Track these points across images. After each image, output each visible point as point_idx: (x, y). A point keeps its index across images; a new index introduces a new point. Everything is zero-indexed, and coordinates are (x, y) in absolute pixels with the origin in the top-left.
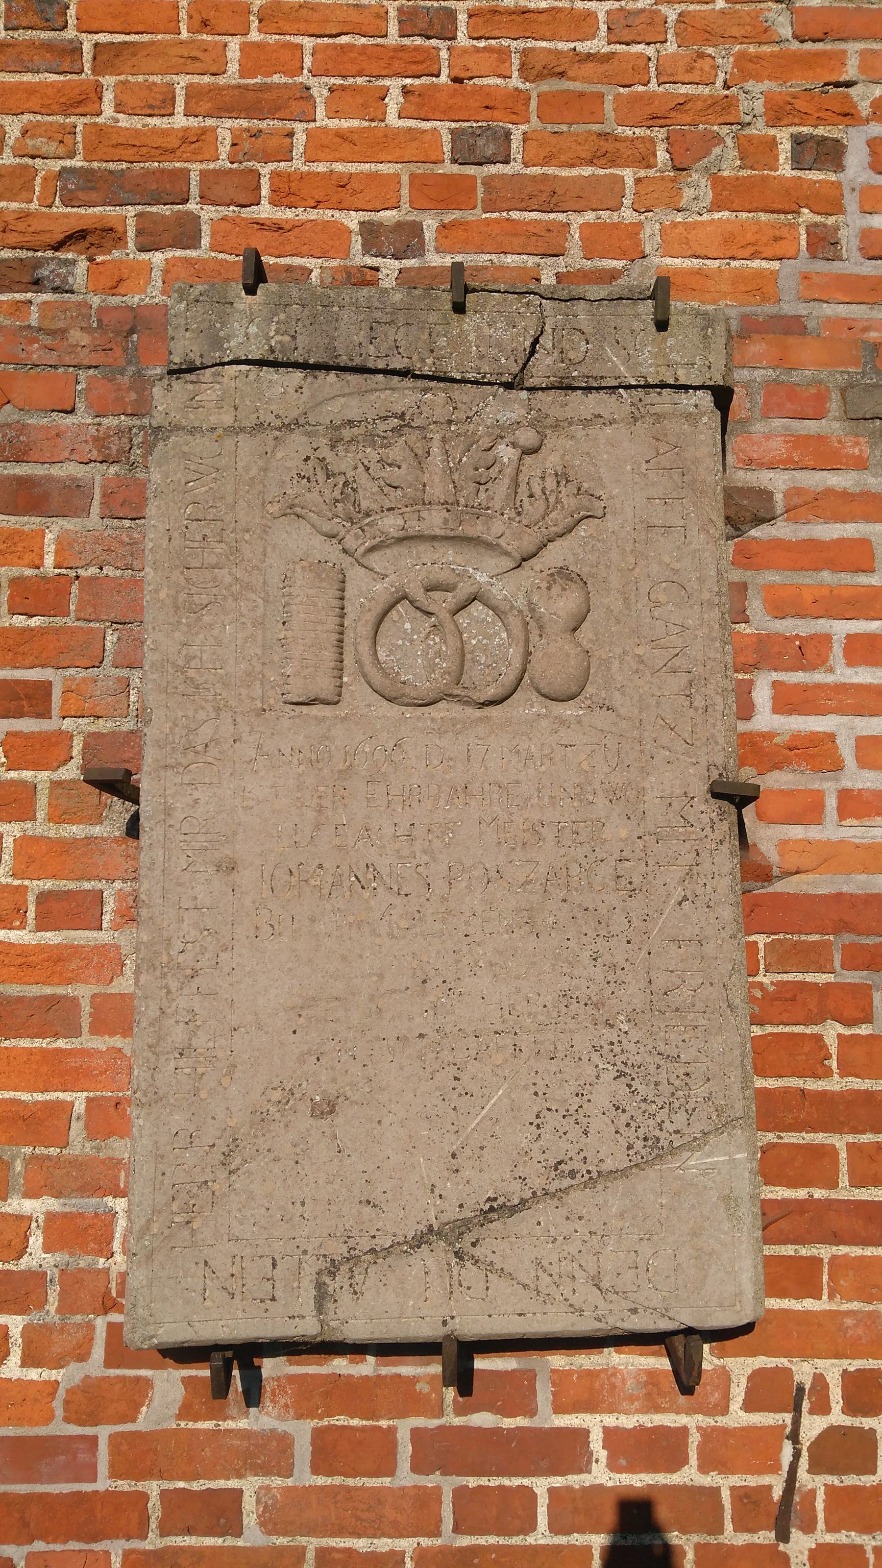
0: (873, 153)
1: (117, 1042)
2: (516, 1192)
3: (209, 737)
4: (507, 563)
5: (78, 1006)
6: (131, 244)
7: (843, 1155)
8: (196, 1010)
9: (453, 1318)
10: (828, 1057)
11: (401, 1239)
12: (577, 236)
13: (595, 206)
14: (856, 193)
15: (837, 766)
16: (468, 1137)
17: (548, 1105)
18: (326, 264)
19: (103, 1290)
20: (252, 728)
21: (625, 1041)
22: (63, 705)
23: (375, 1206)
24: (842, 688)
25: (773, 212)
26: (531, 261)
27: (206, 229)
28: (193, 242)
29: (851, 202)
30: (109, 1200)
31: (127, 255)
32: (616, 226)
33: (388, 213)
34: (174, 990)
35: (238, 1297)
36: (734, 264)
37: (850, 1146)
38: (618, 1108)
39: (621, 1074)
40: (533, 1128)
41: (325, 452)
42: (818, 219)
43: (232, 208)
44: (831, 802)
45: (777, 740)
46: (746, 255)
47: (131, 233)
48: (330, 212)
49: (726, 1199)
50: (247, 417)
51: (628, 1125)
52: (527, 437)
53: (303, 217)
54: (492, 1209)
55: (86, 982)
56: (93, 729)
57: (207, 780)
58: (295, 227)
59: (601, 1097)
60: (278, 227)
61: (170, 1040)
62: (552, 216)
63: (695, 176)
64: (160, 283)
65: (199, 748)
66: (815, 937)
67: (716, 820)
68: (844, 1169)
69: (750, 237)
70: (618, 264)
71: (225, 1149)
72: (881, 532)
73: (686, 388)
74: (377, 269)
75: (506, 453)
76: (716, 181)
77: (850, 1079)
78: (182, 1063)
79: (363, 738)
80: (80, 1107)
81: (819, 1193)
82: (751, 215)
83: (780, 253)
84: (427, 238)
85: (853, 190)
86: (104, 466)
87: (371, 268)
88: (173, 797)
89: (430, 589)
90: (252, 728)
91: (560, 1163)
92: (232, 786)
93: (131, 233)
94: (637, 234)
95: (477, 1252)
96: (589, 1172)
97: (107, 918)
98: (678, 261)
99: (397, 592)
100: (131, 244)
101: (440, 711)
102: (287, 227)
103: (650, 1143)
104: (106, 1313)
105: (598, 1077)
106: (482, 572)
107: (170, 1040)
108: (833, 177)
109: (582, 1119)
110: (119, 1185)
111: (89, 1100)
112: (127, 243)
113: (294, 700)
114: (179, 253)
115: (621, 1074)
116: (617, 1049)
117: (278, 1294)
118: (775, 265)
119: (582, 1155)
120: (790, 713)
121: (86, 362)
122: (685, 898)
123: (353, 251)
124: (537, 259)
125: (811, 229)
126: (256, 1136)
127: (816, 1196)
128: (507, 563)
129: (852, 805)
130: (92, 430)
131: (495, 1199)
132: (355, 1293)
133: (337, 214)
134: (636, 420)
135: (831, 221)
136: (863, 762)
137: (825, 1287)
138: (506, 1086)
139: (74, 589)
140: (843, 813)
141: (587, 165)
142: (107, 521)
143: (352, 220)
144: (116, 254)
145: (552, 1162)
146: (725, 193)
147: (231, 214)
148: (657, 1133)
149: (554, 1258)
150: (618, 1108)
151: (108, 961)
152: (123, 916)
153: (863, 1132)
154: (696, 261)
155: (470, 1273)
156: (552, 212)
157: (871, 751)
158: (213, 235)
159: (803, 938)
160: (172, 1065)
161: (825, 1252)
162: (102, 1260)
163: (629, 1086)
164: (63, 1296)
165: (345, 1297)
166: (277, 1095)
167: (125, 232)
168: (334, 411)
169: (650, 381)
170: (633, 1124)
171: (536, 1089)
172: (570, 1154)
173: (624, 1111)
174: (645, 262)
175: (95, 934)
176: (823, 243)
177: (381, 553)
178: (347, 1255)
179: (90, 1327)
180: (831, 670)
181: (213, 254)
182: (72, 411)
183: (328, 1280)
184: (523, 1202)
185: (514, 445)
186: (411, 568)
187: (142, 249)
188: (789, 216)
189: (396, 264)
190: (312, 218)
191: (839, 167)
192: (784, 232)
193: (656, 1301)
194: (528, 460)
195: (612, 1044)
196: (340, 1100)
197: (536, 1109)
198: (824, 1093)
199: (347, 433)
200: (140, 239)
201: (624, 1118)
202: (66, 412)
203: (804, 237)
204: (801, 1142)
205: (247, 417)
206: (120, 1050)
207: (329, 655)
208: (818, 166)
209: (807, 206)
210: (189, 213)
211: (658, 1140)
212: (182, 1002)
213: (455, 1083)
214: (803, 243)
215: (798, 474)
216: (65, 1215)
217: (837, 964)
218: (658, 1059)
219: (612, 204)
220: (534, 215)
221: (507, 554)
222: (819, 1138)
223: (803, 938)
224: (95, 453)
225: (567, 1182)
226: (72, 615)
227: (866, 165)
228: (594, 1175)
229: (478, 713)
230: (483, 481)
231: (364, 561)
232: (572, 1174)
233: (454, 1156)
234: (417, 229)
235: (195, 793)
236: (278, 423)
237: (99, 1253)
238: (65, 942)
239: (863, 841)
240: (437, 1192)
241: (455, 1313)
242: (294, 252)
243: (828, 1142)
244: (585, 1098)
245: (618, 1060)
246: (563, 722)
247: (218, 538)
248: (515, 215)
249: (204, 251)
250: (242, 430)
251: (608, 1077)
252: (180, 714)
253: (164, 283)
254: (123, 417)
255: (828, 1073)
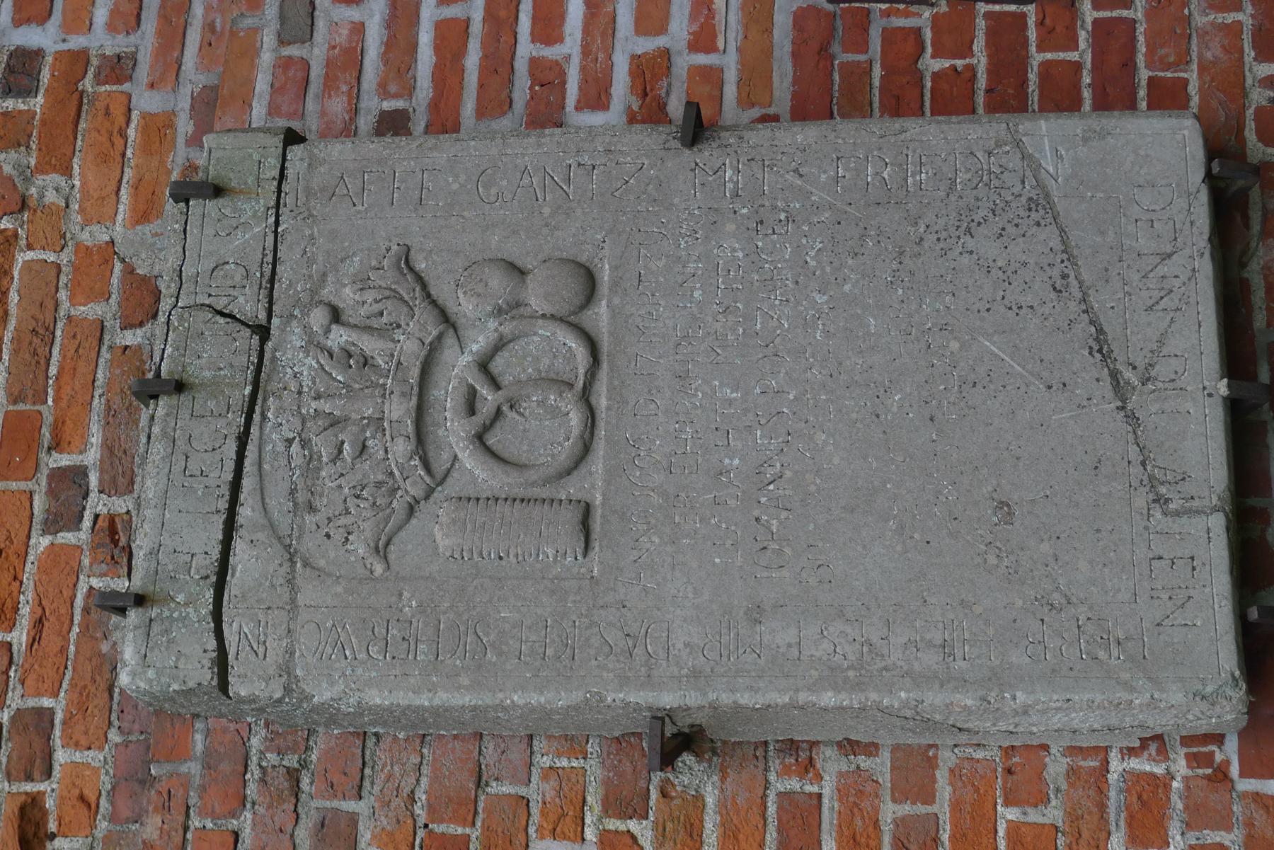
0: (28, 21)
1: (942, 776)
2: (1083, 329)
3: (620, 633)
4: (450, 340)
5: (903, 818)
6: (42, 787)
7: (1049, 56)
8: (905, 640)
9: (1204, 388)
10: (954, 68)
11: (1131, 437)
12: (82, 308)
13: (53, 289)
14: (68, 37)
15: (666, 53)
16: (1032, 374)
17: (999, 298)
18: (86, 570)
19: (1205, 782)
20: (612, 589)
21: (936, 228)
22: (569, 839)
23: (1100, 461)
24: (586, 51)
25: (79, 116)
26: (105, 354)
27: (31, 703)
28: (44, 717)
29: (76, 42)
30: (1113, 777)
31: (53, 790)
32: (76, 269)
33: (36, 503)
34: (883, 664)
35: (1191, 592)
36: (129, 153)
37: (1040, 49)
38: (1001, 235)
39: (968, 231)
40: (1021, 312)
41: (320, 517)
42: (90, 75)
43: (12, 674)
44: (702, 59)
45: (635, 107)
46: (122, 142)
47: (29, 787)
48: (28, 567)
49: (1086, 140)
50: (280, 596)
51: (1017, 225)
52: (318, 318)
53: (30, 595)
54: (1100, 351)
55: (876, 810)
56: (597, 809)
57: (665, 635)
58: (40, 604)
59: (990, 249)
60: (39, 624)
61: (935, 667)
62: (58, 333)
63: (33, 190)
64: (91, 753)
65: (630, 643)
66: (836, 77)
67: (718, 142)
68: (1061, 55)
69: (104, 139)
70: (118, 267)
71: (1046, 609)
72: (429, 12)
73: (283, 169)
74: (97, 516)
75: (339, 337)
76: (41, 169)
77: (975, 48)
78: (959, 654)
79: (624, 478)
80: (1012, 814)
81: (1086, 79)
82: (80, 138)
83: (123, 109)
84: (68, 463)
85: (64, 41)
86: (303, 797)
87: (95, 523)
88: (682, 668)
89: (471, 410)
90: (612, 589)
91: (1055, 289)
92: (672, 609)
93: (29, 787)
94: (87, 248)
95: (1141, 365)
96: (1062, 261)
97: (809, 788)
98: (121, 208)
99: (474, 444)
100: (42, 787)
101: (602, 401)
102: (39, 611)
103: (1033, 206)
104: (1232, 781)
105: (971, 252)
106: (458, 366)
107: (935, 667)
108: (49, 59)
109: (1011, 269)
110: (1094, 768)
111: (1007, 803)
112: (39, 792)
113: (583, 545)
114: (57, 732)
115: (968, 231)
116: (944, 235)
117: (1187, 554)
118: (135, 115)
119: (1046, 268)
120: (609, 95)
121: (181, 819)
122: (796, 171)
123: (73, 541)
124: (104, 349)
125: (98, 81)
126: (1033, 578)
127: (1088, 81)
128: (450, 340)
129: (703, 40)
130: (261, 810)
131: (1091, 348)
132: (1184, 479)
133: (31, 558)
134: (311, 215)
135: (95, 62)
136: (662, 29)
137: (1176, 75)
138: (981, 339)
139: (438, 828)
140: (710, 48)
141: (7, 298)
142: (365, 793)
143: (41, 542)
144: (50, 803)
145: (1053, 295)
146: (53, 161)
147: (19, 674)
148: (1024, 200)
149: (1144, 293)
150: (1001, 235)
151: (857, 792)
152: (807, 771)
153: (1026, 39)
154: (123, 191)
155: (1163, 370)
156: (53, 333)
157: (652, 17)
158: (39, 694)
159: (836, 87)
160: (960, 663)
161: (1144, 74)
162: (1175, 784)
163: (979, 224)
164: (1215, 827)
165: (1189, 488)
166: (992, 560)
167: (27, 794)
168: (278, 502)
169: (272, 203)
170: (1016, 221)
171: (983, 310)
172: (1046, 279)
173: (1003, 229)
174: (118, 240)
175: (825, 801)
176: (118, 68)
177: (432, 460)
178: (1148, 488)
179: (1244, 795)
180: (568, 58)
181: (62, 694)
182: (236, 835)
183: (1172, 506)
184: (1091, 322)
185: (328, 331)
186: (453, 432)
187: (48, 774)
188: (85, 101)
189: (93, 496)
190: (32, 583)
191: (39, 53)
192: (100, 105)
193: (1181, 203)
194: (344, 318)
195: (938, 239)
196: (995, 496)
197: (1002, 309)
198: (990, 72)
199: (301, 497)
200: (36, 775)
201: (1011, 229)
202: (236, 841)
203: (108, 87)
204: (1037, 92)
205: (280, 596)
206: (952, 771)
207: (536, 510)
208: (35, 72)
209: (76, 84)
210: (13, 719)
211: (1030, 199)
212: (896, 657)
213: (979, 386)
214: (115, 88)
215: (365, 85)
216: (1129, 825)
217: (863, 58)
218: (953, 198)
219: (54, 272)
220: (56, 351)
221: (440, 337)
222: (1033, 77)
223: (836, 87)
224: (285, 806)
225: (1072, 279)
226: (468, 831)
227: (40, 28)
228: (1065, 256)
229: (605, 366)
230: (362, 360)
231: (439, 477)
232: (1065, 276)
233: (1050, 387)
234: (59, 475)
235: (677, 646)
236: (287, 565)
237: (1167, 787)
238: (834, 834)
239: (741, 32)
240: (1085, 403)
241: (1201, 386)
242: (68, 604)
243: (1035, 69)
244: (991, 264)
245: (955, 233)
246: (615, 284)
247: (407, 625)
248: (53, 371)
249: (58, 705)
250: (293, 601)
251: (971, 244)
252: (594, 662)
253: (89, 748)
254: (248, 776)
255: (971, 69)
